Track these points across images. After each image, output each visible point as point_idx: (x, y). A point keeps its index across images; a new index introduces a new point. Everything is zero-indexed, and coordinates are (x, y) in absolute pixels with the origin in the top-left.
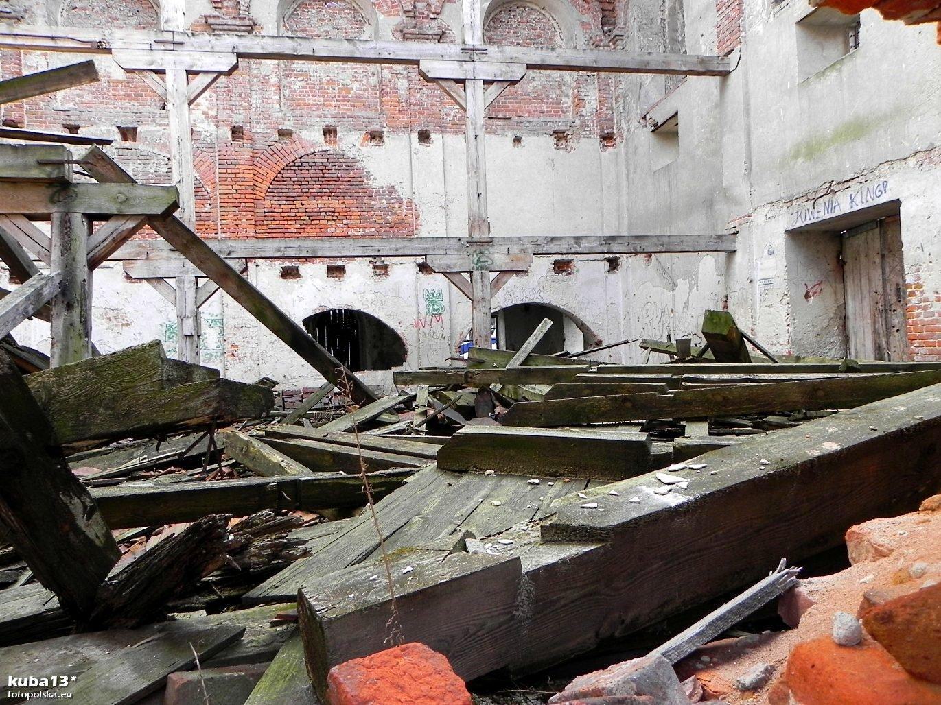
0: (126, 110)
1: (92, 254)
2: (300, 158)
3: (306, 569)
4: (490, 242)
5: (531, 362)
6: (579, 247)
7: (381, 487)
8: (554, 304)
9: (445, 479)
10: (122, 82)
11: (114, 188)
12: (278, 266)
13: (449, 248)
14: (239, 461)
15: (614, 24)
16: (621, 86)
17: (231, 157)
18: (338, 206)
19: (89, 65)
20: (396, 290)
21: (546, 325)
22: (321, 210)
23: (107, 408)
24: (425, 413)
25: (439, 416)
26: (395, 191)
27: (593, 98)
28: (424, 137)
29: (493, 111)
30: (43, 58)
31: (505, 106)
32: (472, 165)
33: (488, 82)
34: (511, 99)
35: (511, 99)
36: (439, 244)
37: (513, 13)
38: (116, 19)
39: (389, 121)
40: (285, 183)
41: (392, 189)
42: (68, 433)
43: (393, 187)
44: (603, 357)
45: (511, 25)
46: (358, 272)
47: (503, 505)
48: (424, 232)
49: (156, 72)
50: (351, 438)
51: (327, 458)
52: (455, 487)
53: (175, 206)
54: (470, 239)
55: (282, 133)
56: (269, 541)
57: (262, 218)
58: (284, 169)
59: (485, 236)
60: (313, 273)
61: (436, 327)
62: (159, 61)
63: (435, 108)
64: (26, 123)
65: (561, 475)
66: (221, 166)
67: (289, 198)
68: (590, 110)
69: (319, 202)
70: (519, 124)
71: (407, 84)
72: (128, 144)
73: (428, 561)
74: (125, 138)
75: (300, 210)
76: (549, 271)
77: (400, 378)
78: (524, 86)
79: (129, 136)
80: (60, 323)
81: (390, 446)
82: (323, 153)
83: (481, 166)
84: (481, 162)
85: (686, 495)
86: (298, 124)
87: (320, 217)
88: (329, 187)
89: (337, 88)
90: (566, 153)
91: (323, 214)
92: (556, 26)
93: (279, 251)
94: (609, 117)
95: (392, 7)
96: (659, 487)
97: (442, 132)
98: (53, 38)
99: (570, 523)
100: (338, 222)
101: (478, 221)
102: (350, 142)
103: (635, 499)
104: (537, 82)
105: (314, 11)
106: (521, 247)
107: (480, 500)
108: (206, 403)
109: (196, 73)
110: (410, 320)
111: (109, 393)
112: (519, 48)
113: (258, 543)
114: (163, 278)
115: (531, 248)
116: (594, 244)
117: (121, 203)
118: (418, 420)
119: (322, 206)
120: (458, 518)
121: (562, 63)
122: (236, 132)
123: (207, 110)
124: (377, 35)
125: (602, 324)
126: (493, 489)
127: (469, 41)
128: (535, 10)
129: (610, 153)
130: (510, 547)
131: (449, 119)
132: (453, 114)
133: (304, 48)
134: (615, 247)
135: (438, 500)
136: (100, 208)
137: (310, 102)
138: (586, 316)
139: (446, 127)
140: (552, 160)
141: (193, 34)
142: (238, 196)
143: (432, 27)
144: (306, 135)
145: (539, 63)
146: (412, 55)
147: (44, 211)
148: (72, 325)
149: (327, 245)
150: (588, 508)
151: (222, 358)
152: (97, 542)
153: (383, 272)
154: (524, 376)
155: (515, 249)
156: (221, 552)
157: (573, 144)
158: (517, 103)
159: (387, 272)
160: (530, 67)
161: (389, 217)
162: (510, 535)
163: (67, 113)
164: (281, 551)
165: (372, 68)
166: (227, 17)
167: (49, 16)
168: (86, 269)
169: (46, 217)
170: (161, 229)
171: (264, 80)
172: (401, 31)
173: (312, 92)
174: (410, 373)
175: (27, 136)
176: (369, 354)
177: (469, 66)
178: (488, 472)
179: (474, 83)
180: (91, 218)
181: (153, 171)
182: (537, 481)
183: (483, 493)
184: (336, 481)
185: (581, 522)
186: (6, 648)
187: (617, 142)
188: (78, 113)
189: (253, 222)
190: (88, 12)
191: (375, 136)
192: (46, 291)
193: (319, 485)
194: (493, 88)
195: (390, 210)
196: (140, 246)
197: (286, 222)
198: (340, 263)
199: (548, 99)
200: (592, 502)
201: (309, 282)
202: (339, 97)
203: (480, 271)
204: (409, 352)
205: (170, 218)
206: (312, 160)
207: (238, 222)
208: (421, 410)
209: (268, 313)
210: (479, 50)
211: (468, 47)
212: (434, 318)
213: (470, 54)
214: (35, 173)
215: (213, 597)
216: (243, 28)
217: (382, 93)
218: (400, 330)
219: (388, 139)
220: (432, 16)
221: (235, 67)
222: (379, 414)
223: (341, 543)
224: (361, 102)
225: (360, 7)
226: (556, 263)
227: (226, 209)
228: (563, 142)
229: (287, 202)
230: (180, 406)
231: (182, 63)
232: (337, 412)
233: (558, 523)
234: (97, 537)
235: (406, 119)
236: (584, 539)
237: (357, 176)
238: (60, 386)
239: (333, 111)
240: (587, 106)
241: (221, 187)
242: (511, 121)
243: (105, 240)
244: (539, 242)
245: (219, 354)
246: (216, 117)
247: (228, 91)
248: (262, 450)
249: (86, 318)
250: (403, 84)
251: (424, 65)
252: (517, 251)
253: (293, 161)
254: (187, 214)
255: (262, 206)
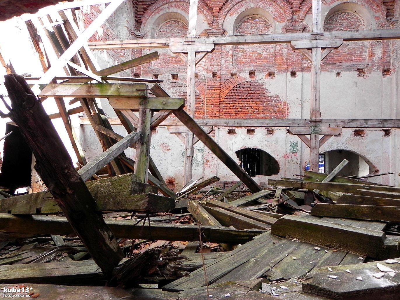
0: (175, 68)
1: (152, 124)
2: (239, 84)
3: (194, 278)
4: (320, 121)
5: (336, 180)
6: (367, 124)
7: (246, 237)
8: (354, 150)
9: (273, 240)
10: (174, 57)
11: (161, 99)
12: (227, 129)
13: (300, 124)
14: (192, 214)
15: (393, 16)
16: (395, 46)
17: (212, 85)
18: (254, 104)
19: (156, 53)
20: (277, 141)
21: (345, 162)
22: (246, 106)
23: (113, 199)
24: (278, 201)
25: (285, 203)
26: (279, 98)
27: (380, 52)
28: (293, 74)
29: (327, 61)
30: (149, 50)
31: (333, 58)
32: (313, 86)
33: (323, 49)
34: (336, 55)
35: (336, 55)
36: (295, 122)
37: (339, 16)
38: (174, 34)
39: (278, 68)
40: (232, 95)
41: (277, 97)
42: (101, 207)
43: (278, 96)
44: (378, 180)
45: (338, 21)
46: (260, 133)
47: (298, 259)
48: (291, 116)
49: (184, 53)
50: (240, 210)
51: (228, 218)
52: (276, 245)
53: (183, 106)
54: (311, 120)
55: (232, 75)
56: (174, 265)
57: (222, 109)
58: (232, 89)
59: (318, 118)
60: (241, 132)
61: (294, 158)
62: (186, 49)
63: (299, 61)
64: (141, 74)
65: (332, 247)
66: (208, 88)
67: (233, 101)
68: (378, 58)
69: (246, 102)
70: (339, 66)
71: (287, 51)
72: (174, 81)
73: (239, 292)
74: (174, 78)
75: (238, 106)
76: (352, 135)
77: (271, 182)
78: (343, 49)
79: (175, 78)
80: (139, 150)
81: (256, 216)
82: (248, 82)
83: (318, 87)
84: (318, 85)
85: (393, 281)
86: (239, 70)
87: (246, 109)
88: (250, 96)
89: (256, 55)
90: (364, 79)
91: (247, 107)
92: (361, 20)
93: (226, 123)
94: (388, 61)
95: (282, 19)
96: (377, 272)
97: (302, 71)
98: (150, 43)
99: (318, 285)
100: (253, 111)
101: (315, 111)
102: (260, 77)
103: (360, 278)
104: (350, 47)
105: (249, 24)
106: (336, 124)
107: (286, 255)
108: (144, 204)
109: (199, 53)
110: (282, 155)
111: (114, 193)
112: (341, 32)
113: (171, 264)
114: (181, 133)
115: (341, 124)
116: (375, 123)
117: (164, 105)
118: (274, 203)
119: (247, 104)
120: (273, 263)
121: (362, 37)
122: (214, 75)
123: (204, 66)
124: (275, 32)
125: (379, 162)
126: (295, 249)
127: (315, 31)
128: (351, 13)
129: (388, 78)
130: (285, 291)
131: (305, 65)
132: (307, 63)
133: (242, 40)
134: (387, 125)
135: (266, 251)
136: (156, 107)
137: (245, 61)
138: (371, 157)
139: (304, 69)
140: (356, 83)
141: (199, 37)
142: (213, 100)
143: (300, 26)
144: (242, 75)
145: (350, 38)
146: (288, 39)
147: (137, 108)
148: (143, 151)
149: (246, 121)
150: (331, 278)
151: (203, 165)
152: (114, 250)
153: (271, 133)
154: (330, 187)
155: (333, 125)
156: (155, 266)
157: (367, 75)
158: (339, 57)
159: (273, 133)
160: (345, 40)
161: (275, 109)
162: (288, 284)
163: (155, 70)
164: (178, 271)
165: (272, 45)
166: (214, 29)
167: (152, 35)
168: (150, 130)
169: (137, 110)
170: (178, 115)
171: (227, 54)
172: (285, 29)
173: (245, 57)
174: (276, 180)
175: (131, 80)
176: (264, 169)
177: (314, 42)
178: (295, 239)
179: (316, 49)
180: (153, 111)
181: (182, 91)
182: (319, 249)
183: (289, 251)
184: (226, 231)
185: (325, 286)
186: (79, 287)
187: (392, 73)
188: (159, 70)
189: (218, 111)
190: (165, 32)
191: (271, 74)
192: (135, 138)
193: (222, 232)
194: (326, 52)
195: (276, 106)
196: (174, 120)
197: (231, 111)
198: (253, 128)
199: (355, 54)
200: (335, 274)
201: (239, 136)
202: (257, 58)
203: (314, 135)
204: (281, 169)
205: (181, 111)
206: (244, 85)
207: (213, 111)
208: (276, 199)
209: (217, 150)
210: (320, 34)
211: (314, 33)
212: (293, 154)
213: (315, 36)
214: (135, 94)
215: (163, 278)
216: (220, 33)
217: (276, 56)
218: (277, 158)
219: (277, 75)
220: (300, 21)
221: (214, 49)
222: (258, 199)
223: (214, 267)
224: (266, 60)
225: (268, 20)
226: (356, 131)
227: (208, 105)
228: (362, 74)
229: (233, 103)
230: (135, 203)
231: (194, 49)
232: (241, 194)
233: (312, 284)
234: (114, 248)
235: (286, 66)
236: (325, 296)
237: (262, 91)
238: (101, 187)
239: (254, 64)
240: (376, 56)
241: (207, 97)
242: (336, 65)
243: (157, 119)
244: (345, 122)
245: (202, 164)
246: (207, 69)
247: (212, 58)
248: (201, 212)
249: (148, 149)
250: (285, 51)
251: (293, 43)
252: (334, 126)
253: (236, 86)
254: (190, 109)
255: (223, 104)
